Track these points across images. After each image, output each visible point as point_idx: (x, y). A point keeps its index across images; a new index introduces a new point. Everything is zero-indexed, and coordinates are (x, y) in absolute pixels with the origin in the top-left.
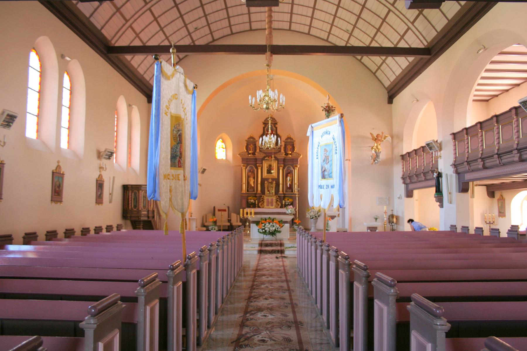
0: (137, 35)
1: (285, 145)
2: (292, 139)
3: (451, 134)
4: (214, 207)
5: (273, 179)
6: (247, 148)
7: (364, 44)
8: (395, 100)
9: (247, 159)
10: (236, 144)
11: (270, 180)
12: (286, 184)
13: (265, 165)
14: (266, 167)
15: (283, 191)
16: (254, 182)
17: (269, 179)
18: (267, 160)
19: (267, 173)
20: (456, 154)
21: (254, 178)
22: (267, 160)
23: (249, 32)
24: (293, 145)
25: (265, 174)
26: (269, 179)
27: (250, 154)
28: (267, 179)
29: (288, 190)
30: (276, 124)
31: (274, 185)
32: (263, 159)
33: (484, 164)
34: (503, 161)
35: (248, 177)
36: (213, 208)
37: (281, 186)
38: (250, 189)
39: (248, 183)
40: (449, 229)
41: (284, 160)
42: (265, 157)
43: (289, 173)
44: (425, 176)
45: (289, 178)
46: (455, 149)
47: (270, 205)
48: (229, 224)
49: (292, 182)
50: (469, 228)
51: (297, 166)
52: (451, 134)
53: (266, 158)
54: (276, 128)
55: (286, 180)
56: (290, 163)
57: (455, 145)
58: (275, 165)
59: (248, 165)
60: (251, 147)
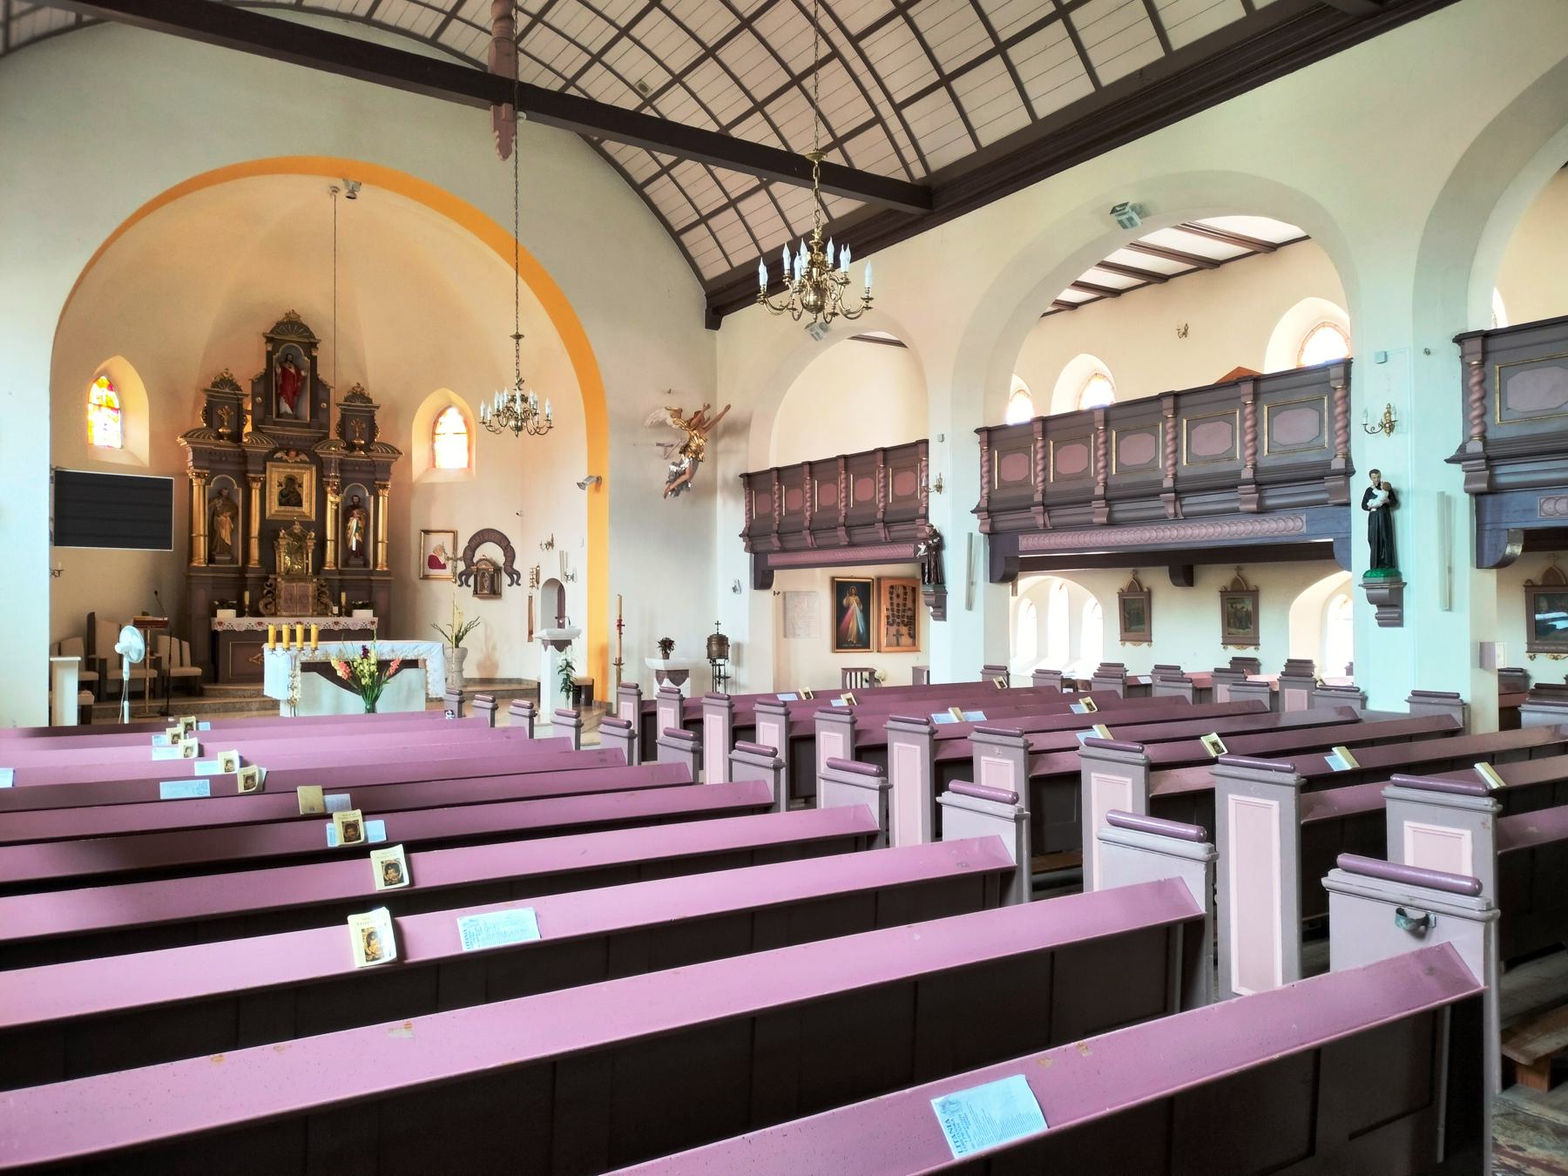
0: (537, 18)
1: (344, 417)
2: (370, 401)
3: (978, 431)
4: (91, 617)
5: (307, 525)
6: (209, 414)
7: (655, 158)
8: (727, 320)
9: (211, 452)
10: (164, 395)
11: (297, 528)
12: (346, 540)
13: (275, 476)
14: (275, 483)
15: (336, 564)
16: (233, 532)
17: (293, 523)
18: (281, 460)
19: (281, 504)
20: (990, 482)
21: (234, 518)
22: (281, 460)
23: (77, 32)
24: (372, 418)
25: (273, 507)
26: (293, 523)
27: (221, 436)
28: (288, 525)
29: (353, 561)
30: (314, 345)
31: (311, 544)
32: (269, 457)
33: (1110, 512)
34: (1185, 509)
35: (213, 515)
36: (85, 619)
37: (330, 546)
38: (221, 553)
39: (212, 533)
40: (978, 678)
41: (342, 466)
42: (275, 451)
43: (355, 507)
44: (848, 534)
45: (353, 523)
46: (990, 471)
47: (880, 628)
48: (154, 673)
49: (365, 535)
50: (1012, 672)
51: (385, 487)
52: (978, 431)
53: (278, 455)
54: (314, 360)
55: (346, 528)
56: (360, 476)
57: (991, 460)
58: (308, 480)
59: (214, 473)
60: (224, 412)
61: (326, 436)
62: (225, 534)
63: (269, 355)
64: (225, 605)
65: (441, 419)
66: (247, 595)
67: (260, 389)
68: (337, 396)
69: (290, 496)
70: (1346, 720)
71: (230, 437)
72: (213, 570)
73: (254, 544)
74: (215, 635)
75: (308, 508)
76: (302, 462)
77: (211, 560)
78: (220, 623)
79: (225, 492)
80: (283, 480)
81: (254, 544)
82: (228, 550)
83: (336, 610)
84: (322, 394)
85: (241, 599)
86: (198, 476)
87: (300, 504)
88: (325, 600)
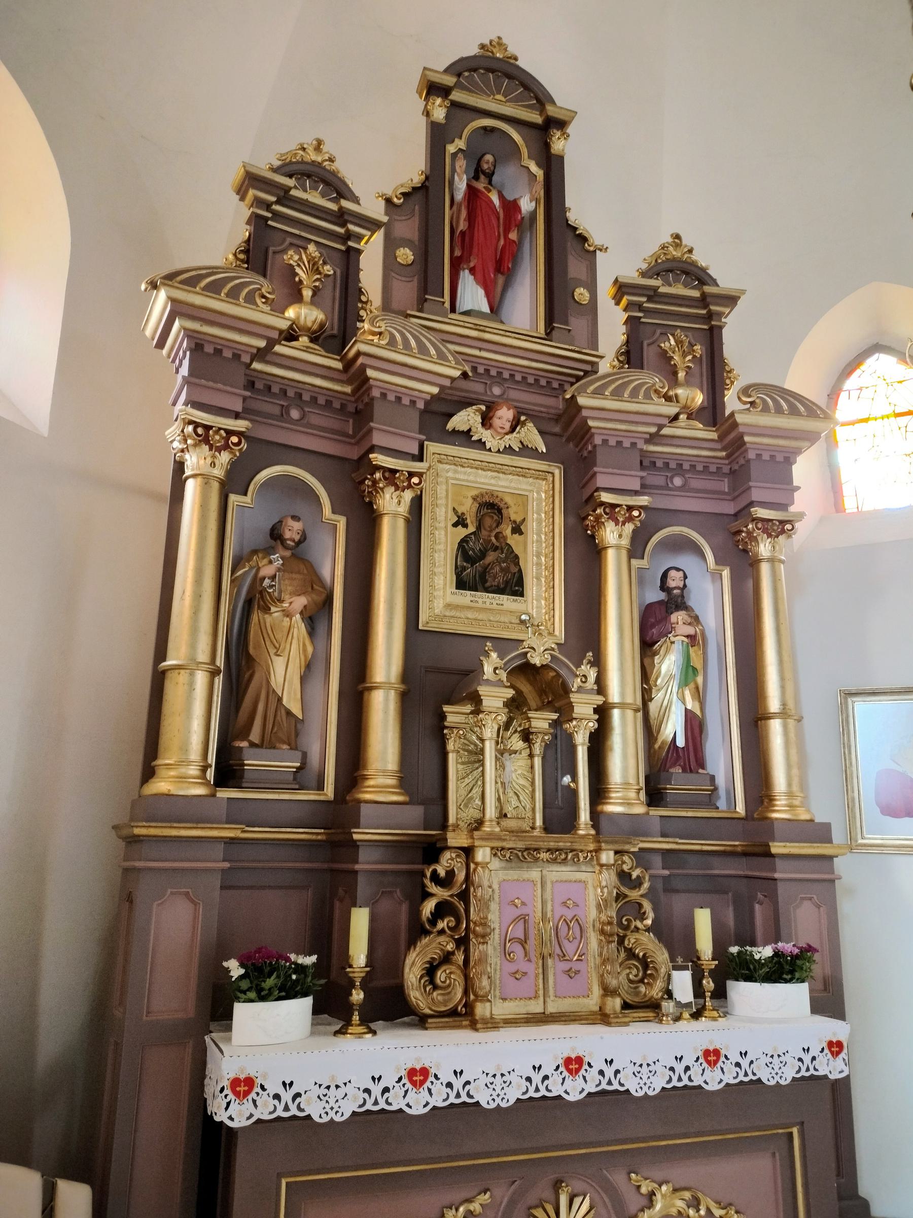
18: (465, 437)
21: (316, 618)
22: (465, 437)
32: (435, 417)
38: (267, 743)
39: (239, 670)
54: (553, 167)
61: (592, 369)
62: (283, 672)
63: (438, 136)
64: (270, 980)
65: (851, 383)
66: (360, 921)
67: (409, 228)
68: (620, 259)
69: (487, 565)
70: (497, 815)
71: (317, 336)
72: (236, 813)
73: (383, 710)
74: (213, 1145)
75: (543, 605)
76: (526, 451)
77: (228, 771)
78: (244, 1086)
79: (292, 530)
80: (468, 507)
81: (383, 710)
82: (288, 731)
83: (682, 984)
84: (575, 268)
85: (328, 937)
86: (204, 435)
87: (514, 586)
88: (646, 942)
